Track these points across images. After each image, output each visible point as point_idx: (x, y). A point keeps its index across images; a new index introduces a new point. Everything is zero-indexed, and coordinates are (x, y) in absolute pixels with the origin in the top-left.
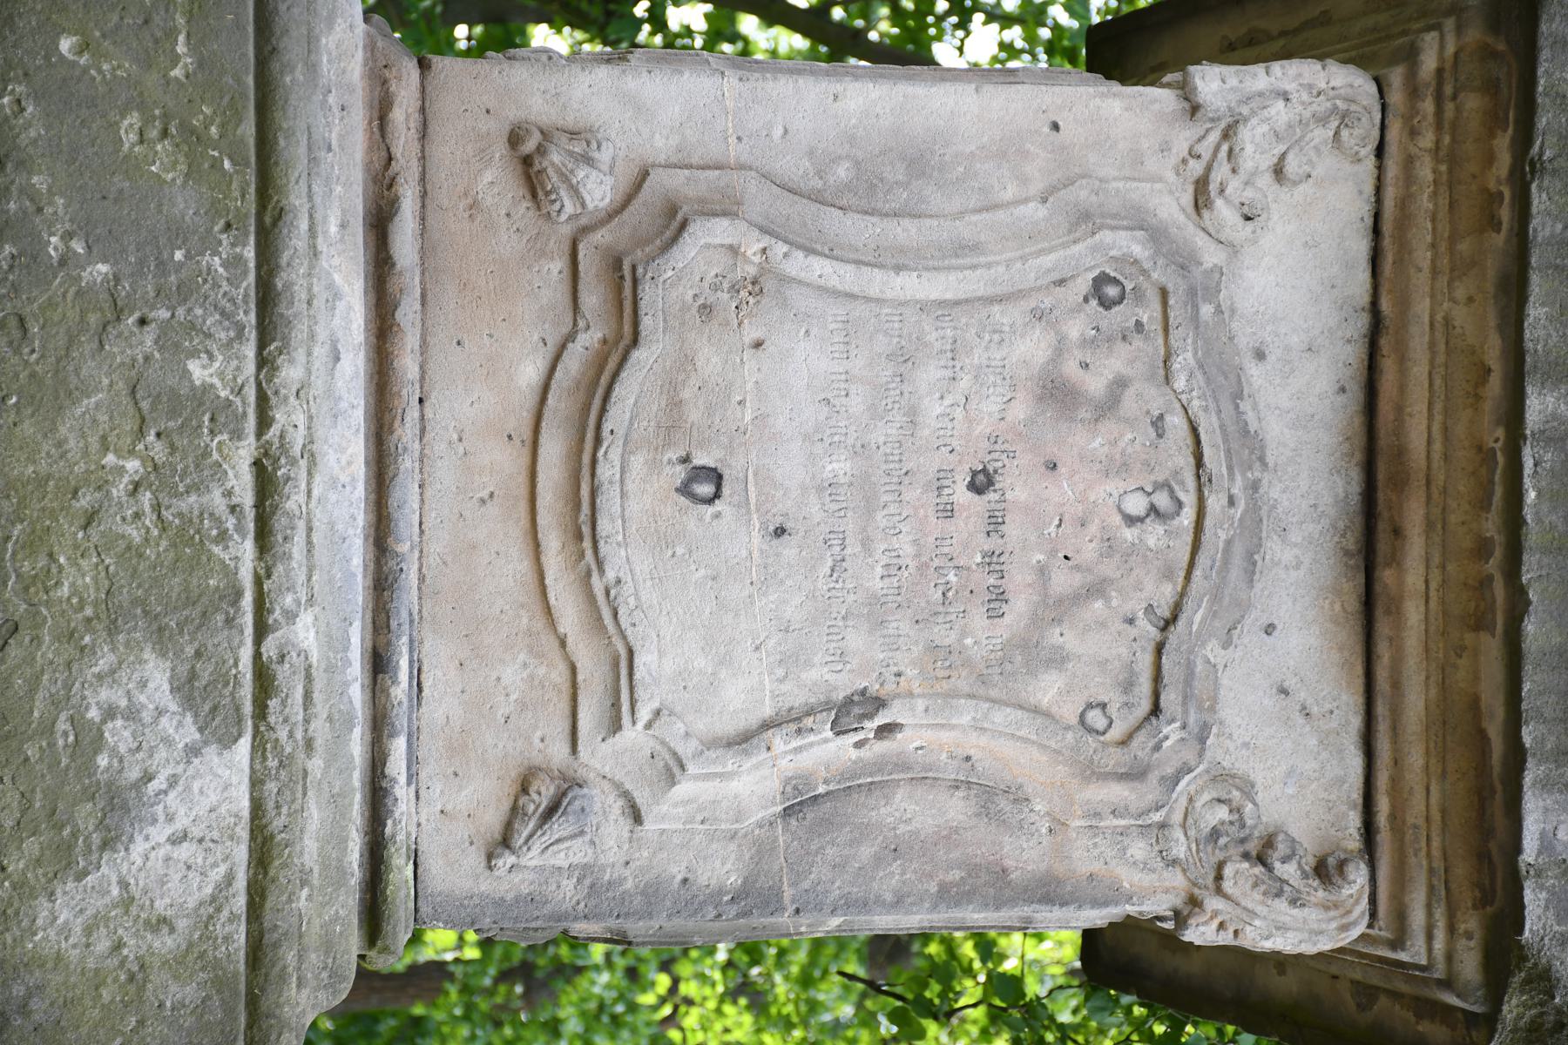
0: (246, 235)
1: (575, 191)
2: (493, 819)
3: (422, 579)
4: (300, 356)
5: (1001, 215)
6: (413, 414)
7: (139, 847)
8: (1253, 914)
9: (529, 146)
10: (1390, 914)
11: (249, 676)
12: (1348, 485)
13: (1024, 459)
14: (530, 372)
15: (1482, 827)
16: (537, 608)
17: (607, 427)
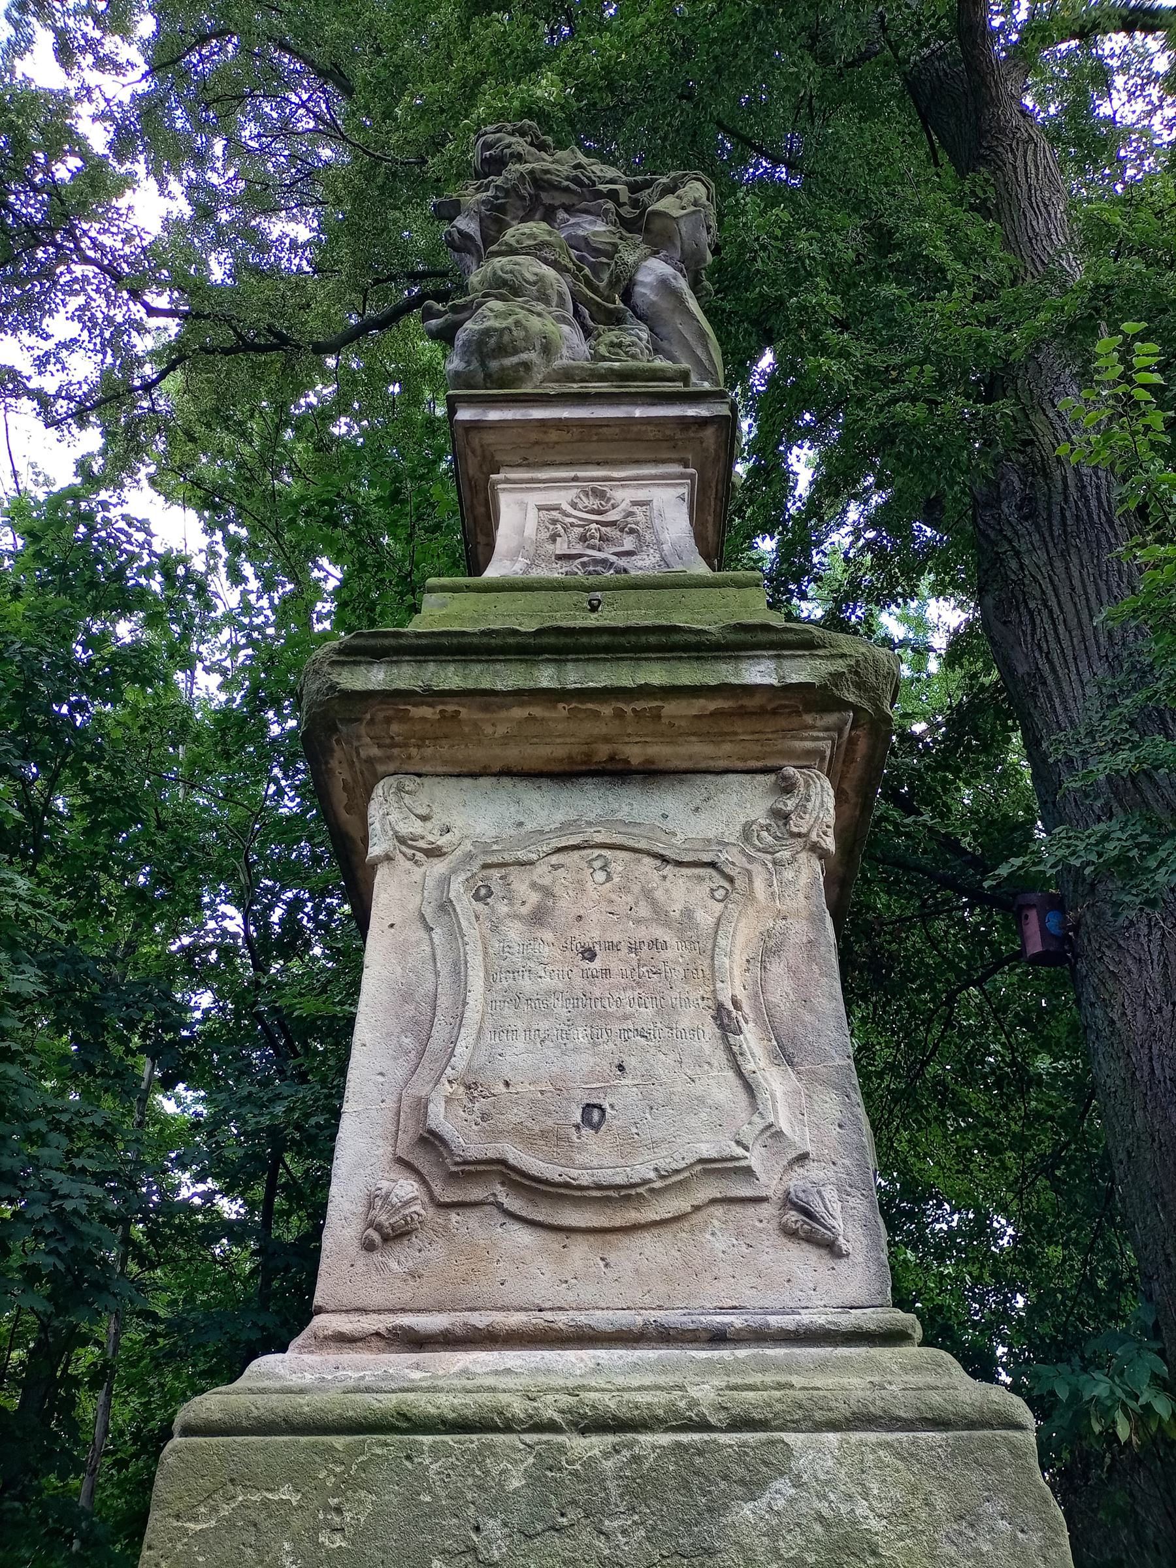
0: (415, 1442)
1: (406, 1204)
2: (813, 1256)
3: (660, 1308)
4: (504, 1398)
5: (438, 952)
6: (549, 1315)
7: (875, 1524)
8: (817, 817)
9: (376, 1237)
10: (808, 758)
11: (739, 1435)
12: (589, 784)
13: (576, 932)
14: (523, 1236)
15: (760, 713)
16: (675, 1226)
17: (558, 1179)
